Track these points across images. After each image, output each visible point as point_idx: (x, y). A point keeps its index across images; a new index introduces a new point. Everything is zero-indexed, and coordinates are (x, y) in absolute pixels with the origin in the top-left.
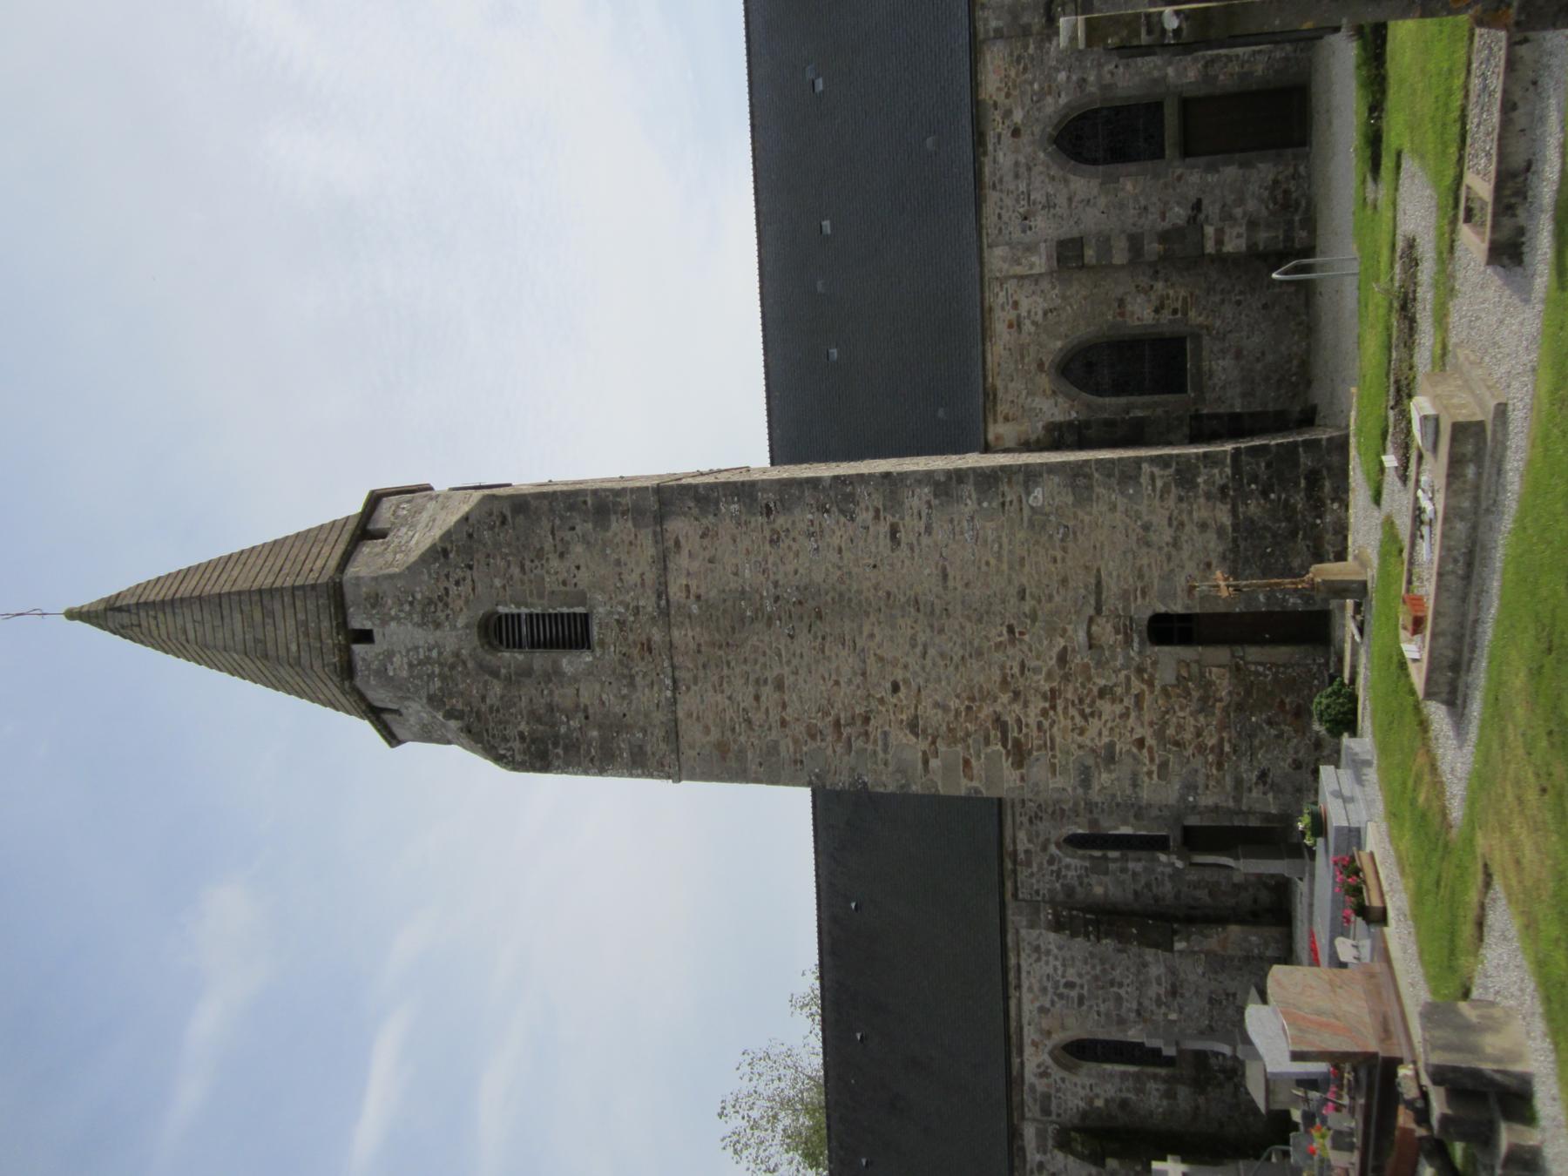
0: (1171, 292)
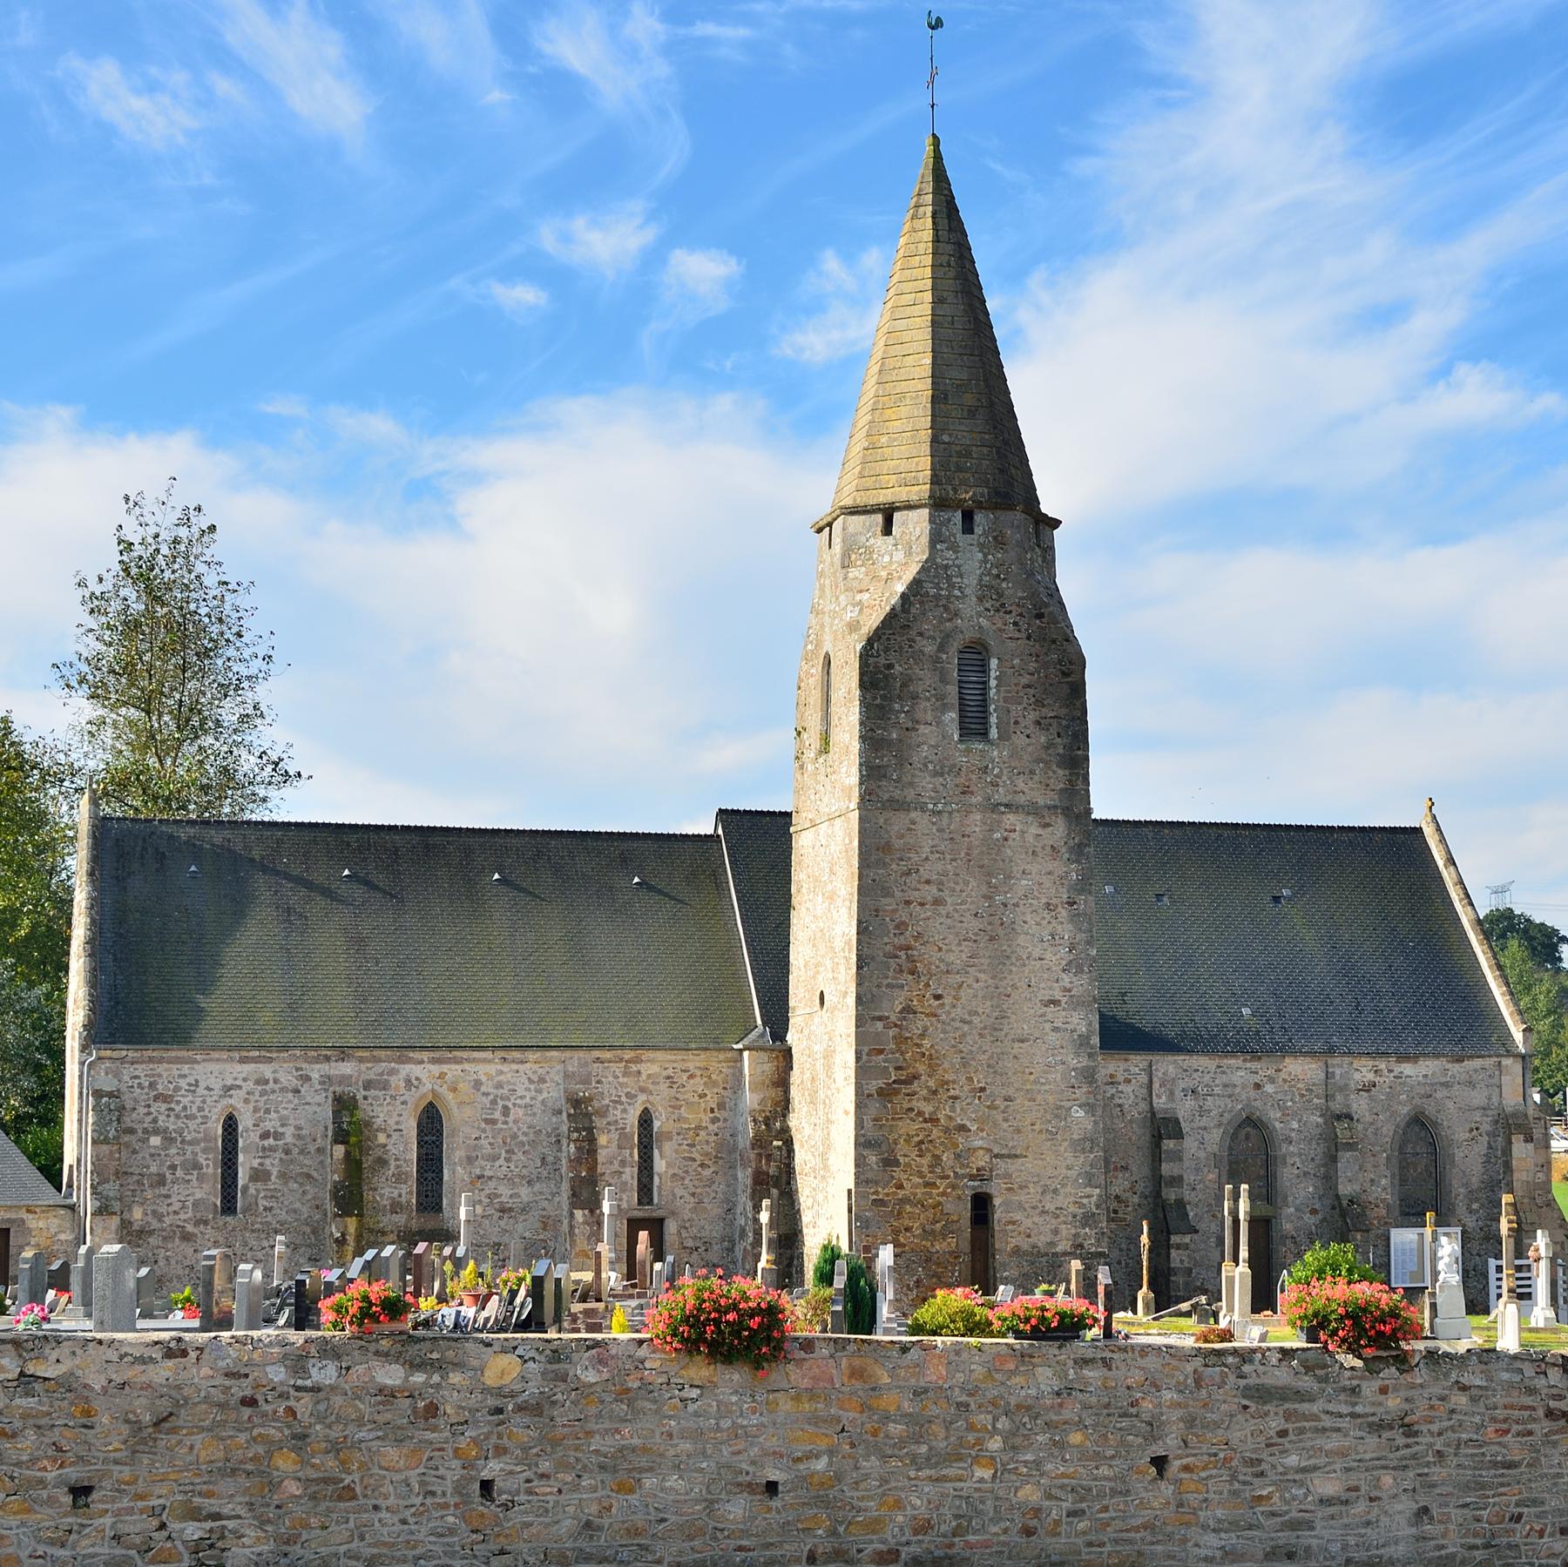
0: (1130, 1209)
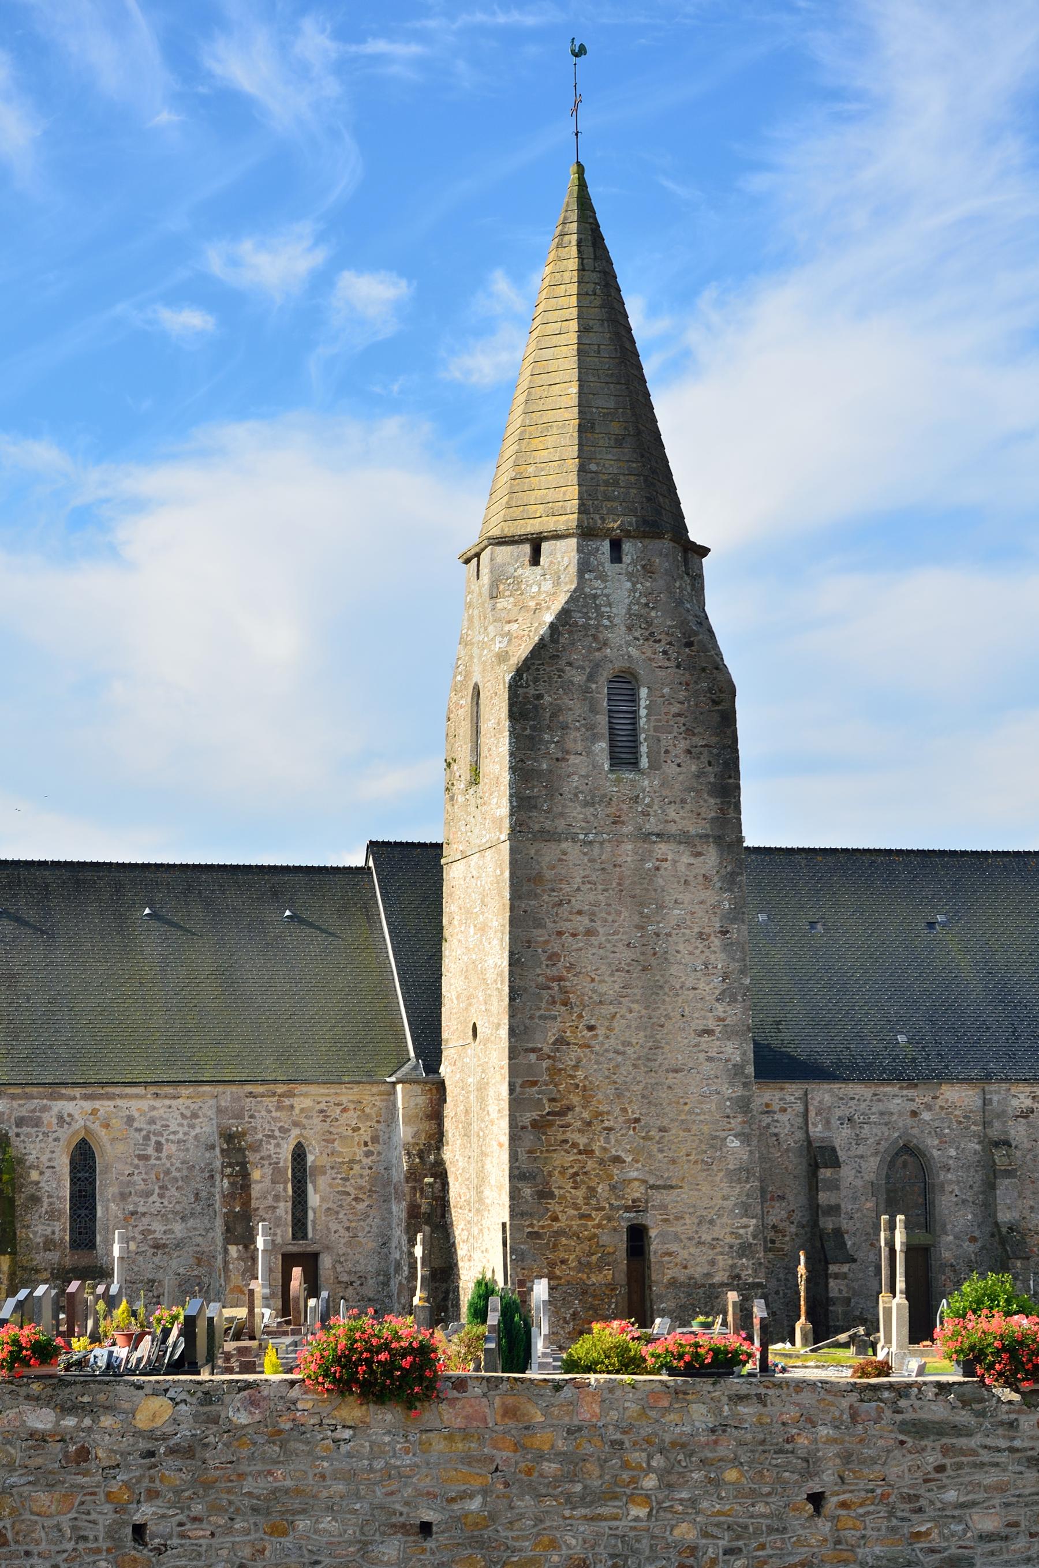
0: (787, 1238)
